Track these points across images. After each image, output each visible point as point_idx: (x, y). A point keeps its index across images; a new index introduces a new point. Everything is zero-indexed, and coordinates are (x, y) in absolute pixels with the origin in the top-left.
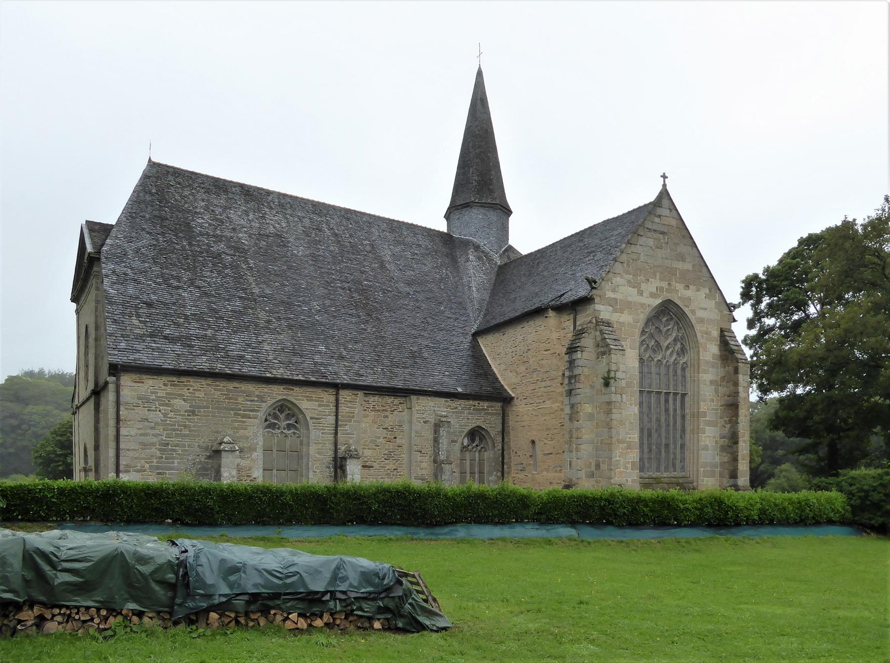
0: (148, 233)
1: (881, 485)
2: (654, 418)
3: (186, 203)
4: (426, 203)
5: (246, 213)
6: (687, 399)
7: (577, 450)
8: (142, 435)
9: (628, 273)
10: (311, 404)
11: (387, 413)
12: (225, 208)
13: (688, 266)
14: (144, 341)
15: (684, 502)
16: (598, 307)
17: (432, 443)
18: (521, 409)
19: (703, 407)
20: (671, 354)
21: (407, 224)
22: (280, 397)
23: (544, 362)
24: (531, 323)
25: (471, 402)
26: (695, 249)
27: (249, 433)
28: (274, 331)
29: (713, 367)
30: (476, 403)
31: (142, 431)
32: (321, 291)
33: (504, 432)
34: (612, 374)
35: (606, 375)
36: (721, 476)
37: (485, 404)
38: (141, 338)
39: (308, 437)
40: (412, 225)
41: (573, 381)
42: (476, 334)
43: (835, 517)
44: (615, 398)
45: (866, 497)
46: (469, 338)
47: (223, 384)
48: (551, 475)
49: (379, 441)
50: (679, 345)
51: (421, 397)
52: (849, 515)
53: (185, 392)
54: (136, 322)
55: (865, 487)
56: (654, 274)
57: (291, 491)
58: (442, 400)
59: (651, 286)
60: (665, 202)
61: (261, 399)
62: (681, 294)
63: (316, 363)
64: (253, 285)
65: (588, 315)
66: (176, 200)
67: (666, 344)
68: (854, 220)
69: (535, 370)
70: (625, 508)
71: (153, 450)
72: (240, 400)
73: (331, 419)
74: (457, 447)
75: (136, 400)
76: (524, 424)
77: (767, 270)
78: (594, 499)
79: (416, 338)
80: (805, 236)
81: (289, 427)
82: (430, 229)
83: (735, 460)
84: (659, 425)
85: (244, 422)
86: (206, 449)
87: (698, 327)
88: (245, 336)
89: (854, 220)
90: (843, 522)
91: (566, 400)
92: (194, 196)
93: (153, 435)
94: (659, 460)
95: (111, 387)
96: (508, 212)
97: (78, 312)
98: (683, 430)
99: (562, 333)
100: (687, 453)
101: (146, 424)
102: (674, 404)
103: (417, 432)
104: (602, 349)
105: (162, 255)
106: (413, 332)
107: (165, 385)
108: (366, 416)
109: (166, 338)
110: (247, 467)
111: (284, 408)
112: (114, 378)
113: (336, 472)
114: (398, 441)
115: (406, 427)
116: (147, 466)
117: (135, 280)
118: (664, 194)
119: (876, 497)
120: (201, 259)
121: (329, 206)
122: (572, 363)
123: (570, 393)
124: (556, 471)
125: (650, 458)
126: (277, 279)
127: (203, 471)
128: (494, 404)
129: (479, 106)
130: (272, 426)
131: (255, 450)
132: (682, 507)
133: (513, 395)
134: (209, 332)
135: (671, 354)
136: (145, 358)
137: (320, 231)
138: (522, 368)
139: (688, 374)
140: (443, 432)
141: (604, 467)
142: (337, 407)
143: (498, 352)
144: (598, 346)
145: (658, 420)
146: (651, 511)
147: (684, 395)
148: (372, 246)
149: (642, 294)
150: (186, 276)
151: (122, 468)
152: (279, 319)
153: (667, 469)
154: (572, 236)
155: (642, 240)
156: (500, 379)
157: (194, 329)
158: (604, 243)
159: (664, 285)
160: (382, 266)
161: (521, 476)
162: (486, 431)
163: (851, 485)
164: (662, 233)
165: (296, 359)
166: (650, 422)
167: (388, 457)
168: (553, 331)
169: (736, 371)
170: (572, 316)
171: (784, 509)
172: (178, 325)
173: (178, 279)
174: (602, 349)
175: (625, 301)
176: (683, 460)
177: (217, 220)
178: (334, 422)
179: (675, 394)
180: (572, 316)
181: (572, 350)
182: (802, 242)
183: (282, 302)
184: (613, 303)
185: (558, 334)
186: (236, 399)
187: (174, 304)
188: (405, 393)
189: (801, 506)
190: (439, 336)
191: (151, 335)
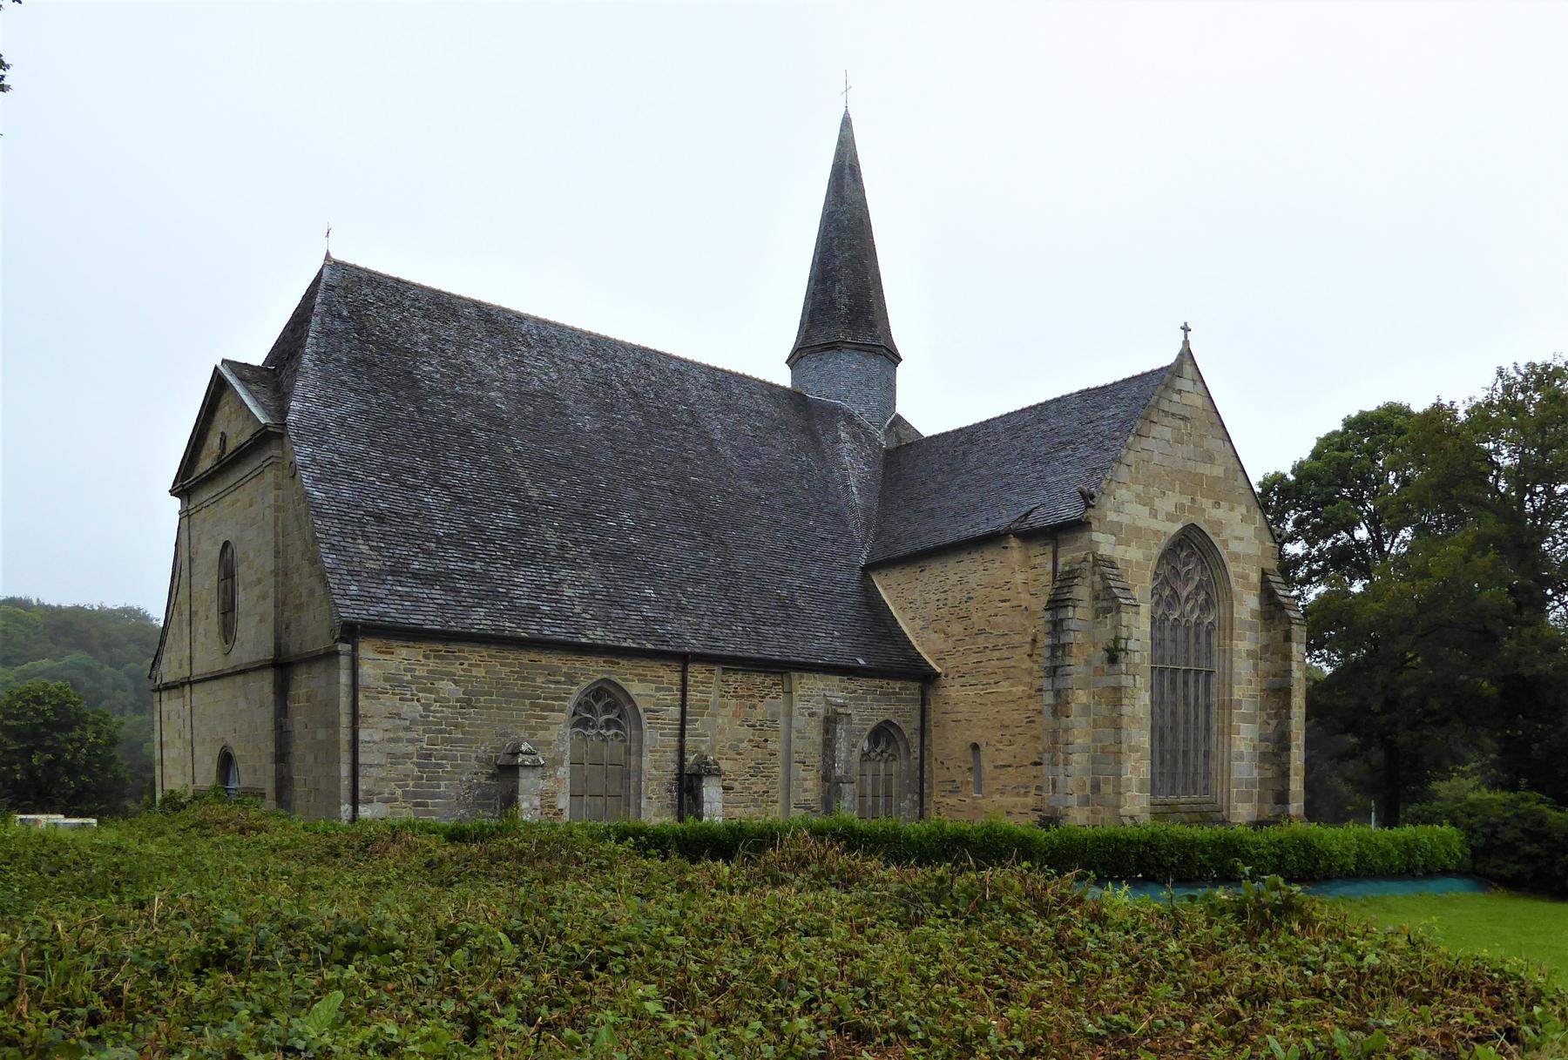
0: (352, 390)
1: (1517, 816)
2: (1168, 710)
3: (398, 335)
4: (751, 331)
5: (493, 355)
6: (1214, 680)
7: (1067, 763)
8: (391, 740)
9: (1136, 482)
10: (647, 688)
11: (755, 701)
12: (461, 346)
13: (1218, 471)
14: (384, 582)
15: (1257, 845)
16: (1097, 536)
17: (820, 749)
18: (954, 693)
19: (1238, 693)
20: (1192, 611)
21: (737, 374)
22: (599, 676)
23: (999, 619)
24: (977, 555)
25: (877, 682)
27: (552, 735)
28: (572, 564)
29: (1251, 629)
30: (884, 682)
31: (391, 735)
32: (631, 494)
33: (923, 731)
34: (1122, 644)
35: (1111, 645)
36: (1261, 800)
37: (897, 685)
38: (377, 576)
39: (640, 741)
40: (743, 376)
41: (1059, 653)
42: (869, 568)
43: (1452, 864)
44: (1126, 681)
45: (1494, 834)
46: (858, 573)
47: (511, 656)
48: (1008, 800)
50: (1202, 597)
52: (1468, 862)
53: (456, 668)
54: (365, 549)
55: (1493, 820)
56: (1172, 482)
57: (676, 837)
58: (835, 680)
59: (1167, 505)
60: (1188, 369)
61: (571, 680)
63: (646, 619)
64: (527, 484)
65: (1078, 549)
66: (382, 331)
67: (1185, 594)
68: (1452, 403)
69: (982, 632)
70: (1173, 855)
71: (409, 765)
72: (539, 680)
73: (675, 711)
74: (857, 753)
75: (382, 683)
76: (959, 717)
77: (1298, 469)
78: (1130, 842)
79: (782, 573)
80: (1354, 414)
81: (609, 724)
82: (771, 385)
83: (1285, 775)
84: (1175, 721)
85: (544, 718)
86: (488, 762)
87: (1232, 568)
88: (531, 571)
89: (1452, 403)
90: (1460, 873)
91: (1046, 683)
92: (409, 323)
93: (409, 741)
94: (1173, 776)
95: (344, 661)
96: (895, 359)
97: (185, 514)
98: (1208, 729)
99: (1031, 574)
100: (1212, 765)
101: (398, 722)
102: (1196, 688)
103: (799, 731)
104: (1105, 604)
105: (381, 429)
106: (776, 563)
107: (426, 657)
108: (724, 706)
109: (415, 575)
112: (349, 647)
113: (680, 798)
114: (770, 746)
115: (782, 723)
116: (399, 792)
117: (350, 474)
118: (1186, 356)
119: (1509, 834)
120: (441, 437)
121: (615, 342)
122: (1057, 626)
123: (1053, 672)
124: (1018, 794)
125: (1162, 774)
126: (563, 473)
127: (483, 800)
128: (909, 684)
129: (848, 178)
130: (584, 723)
131: (561, 763)
132: (1254, 852)
133: (939, 670)
134: (477, 565)
135: (1192, 611)
136: (393, 612)
137: (610, 386)
138: (957, 628)
139: (1214, 641)
140: (840, 731)
141: (1107, 789)
142: (684, 691)
143: (910, 601)
144: (1096, 598)
145: (1174, 713)
146: (1210, 859)
147: (1209, 674)
148: (691, 413)
149: (1155, 516)
150: (424, 466)
151: (361, 795)
152: (576, 543)
153: (1185, 792)
154: (1023, 410)
155: (1156, 430)
156: (914, 643)
157: (454, 561)
158: (1088, 429)
159: (1186, 500)
160: (712, 450)
161: (952, 800)
162: (899, 729)
163: (1470, 816)
164: (1184, 418)
165: (617, 612)
166: (1162, 716)
167: (756, 771)
168: (1018, 574)
169: (1288, 638)
170: (1050, 549)
171: (1388, 853)
172: (429, 554)
173: (414, 472)
174: (1105, 604)
175: (1132, 526)
176: (1207, 775)
177: (452, 366)
178: (678, 716)
179: (1198, 672)
180: (1050, 549)
181: (1057, 603)
182: (1349, 423)
183: (576, 512)
184: (1115, 529)
185: (1023, 576)
186: (534, 680)
187: (415, 516)
188: (781, 668)
189: (1409, 848)
190: (815, 570)
191: (392, 573)
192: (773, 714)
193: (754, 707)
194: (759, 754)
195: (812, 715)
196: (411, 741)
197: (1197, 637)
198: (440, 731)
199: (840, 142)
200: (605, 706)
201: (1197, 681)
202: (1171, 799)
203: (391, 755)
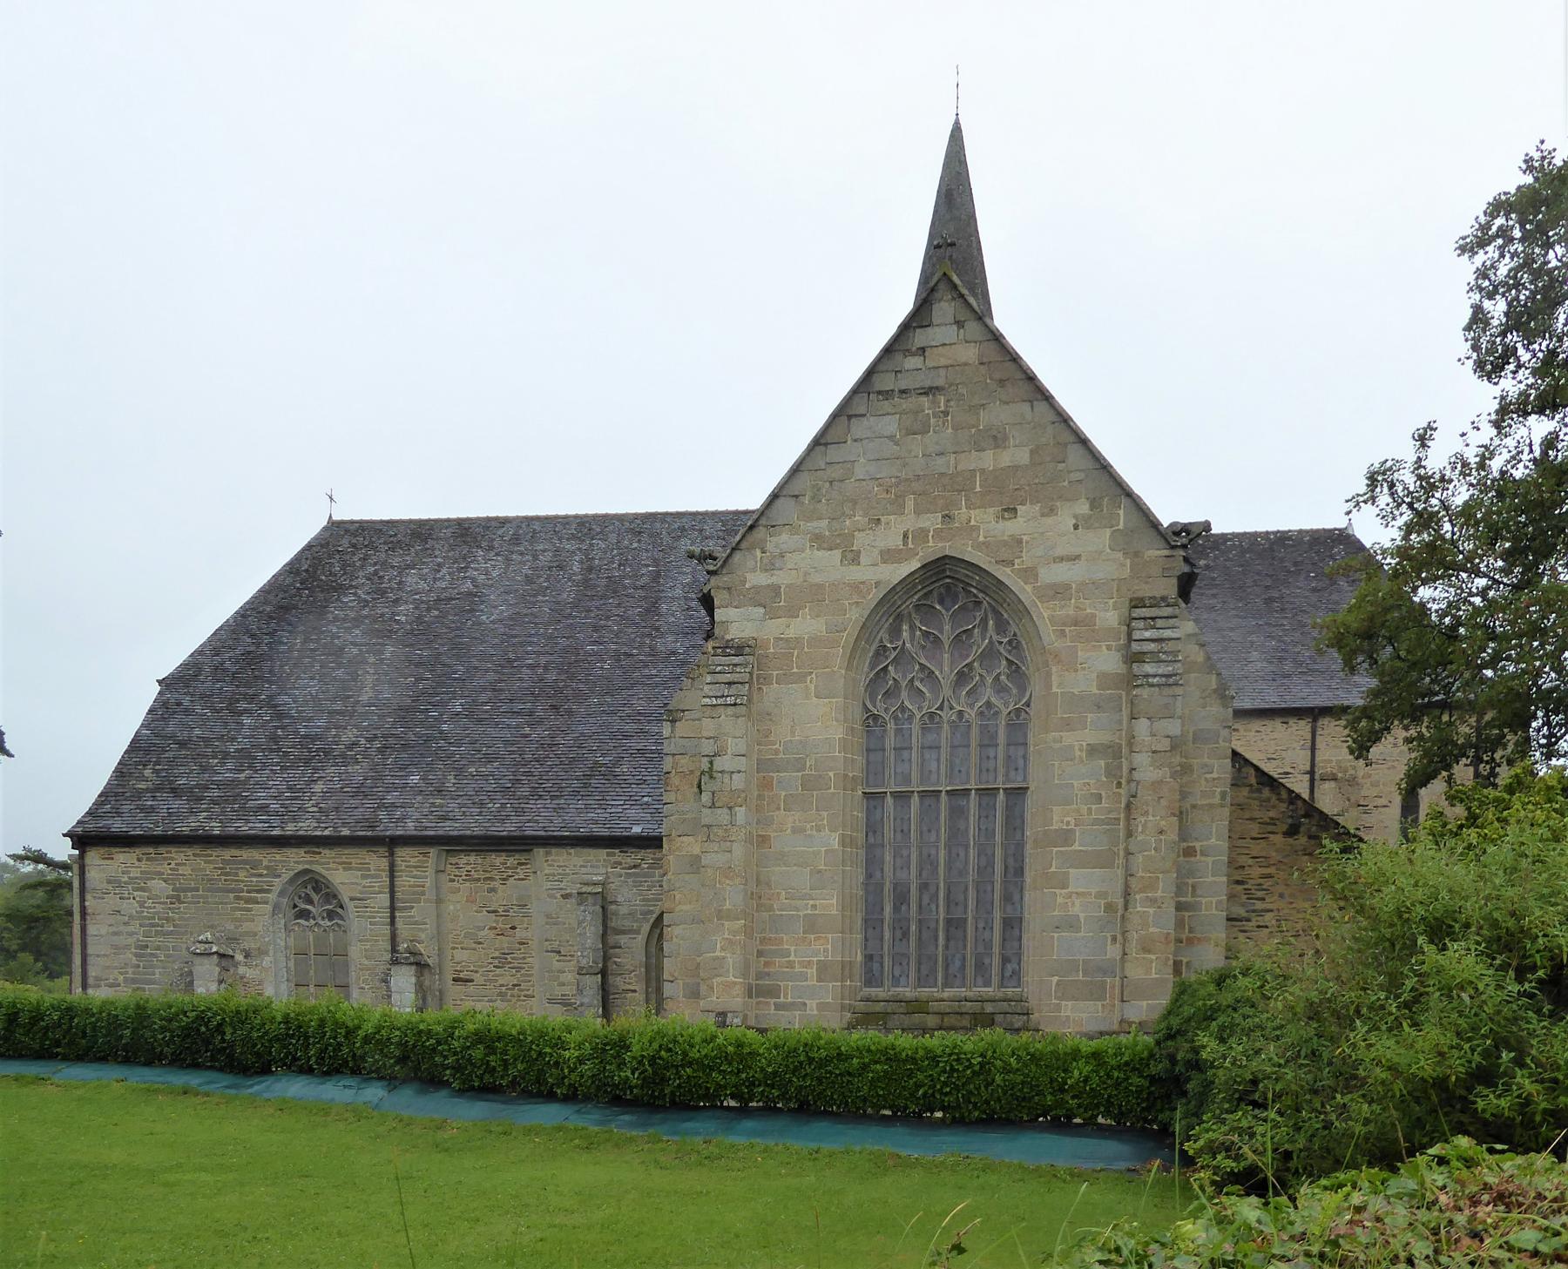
8: (115, 934)
10: (349, 875)
11: (496, 884)
13: (1016, 455)
22: (301, 867)
26: (1041, 407)
49: (482, 933)
51: (554, 850)
53: (165, 868)
58: (602, 853)
62: (980, 534)
72: (242, 875)
73: (385, 899)
85: (249, 910)
110: (272, 984)
111: (313, 885)
114: (520, 934)
131: (266, 953)
142: (392, 877)
147: (1018, 793)
149: (855, 560)
151: (91, 981)
184: (768, 599)
196: (131, 934)
198: (152, 925)
199: (952, 136)
200: (313, 896)
202: (924, 992)
203: (116, 947)
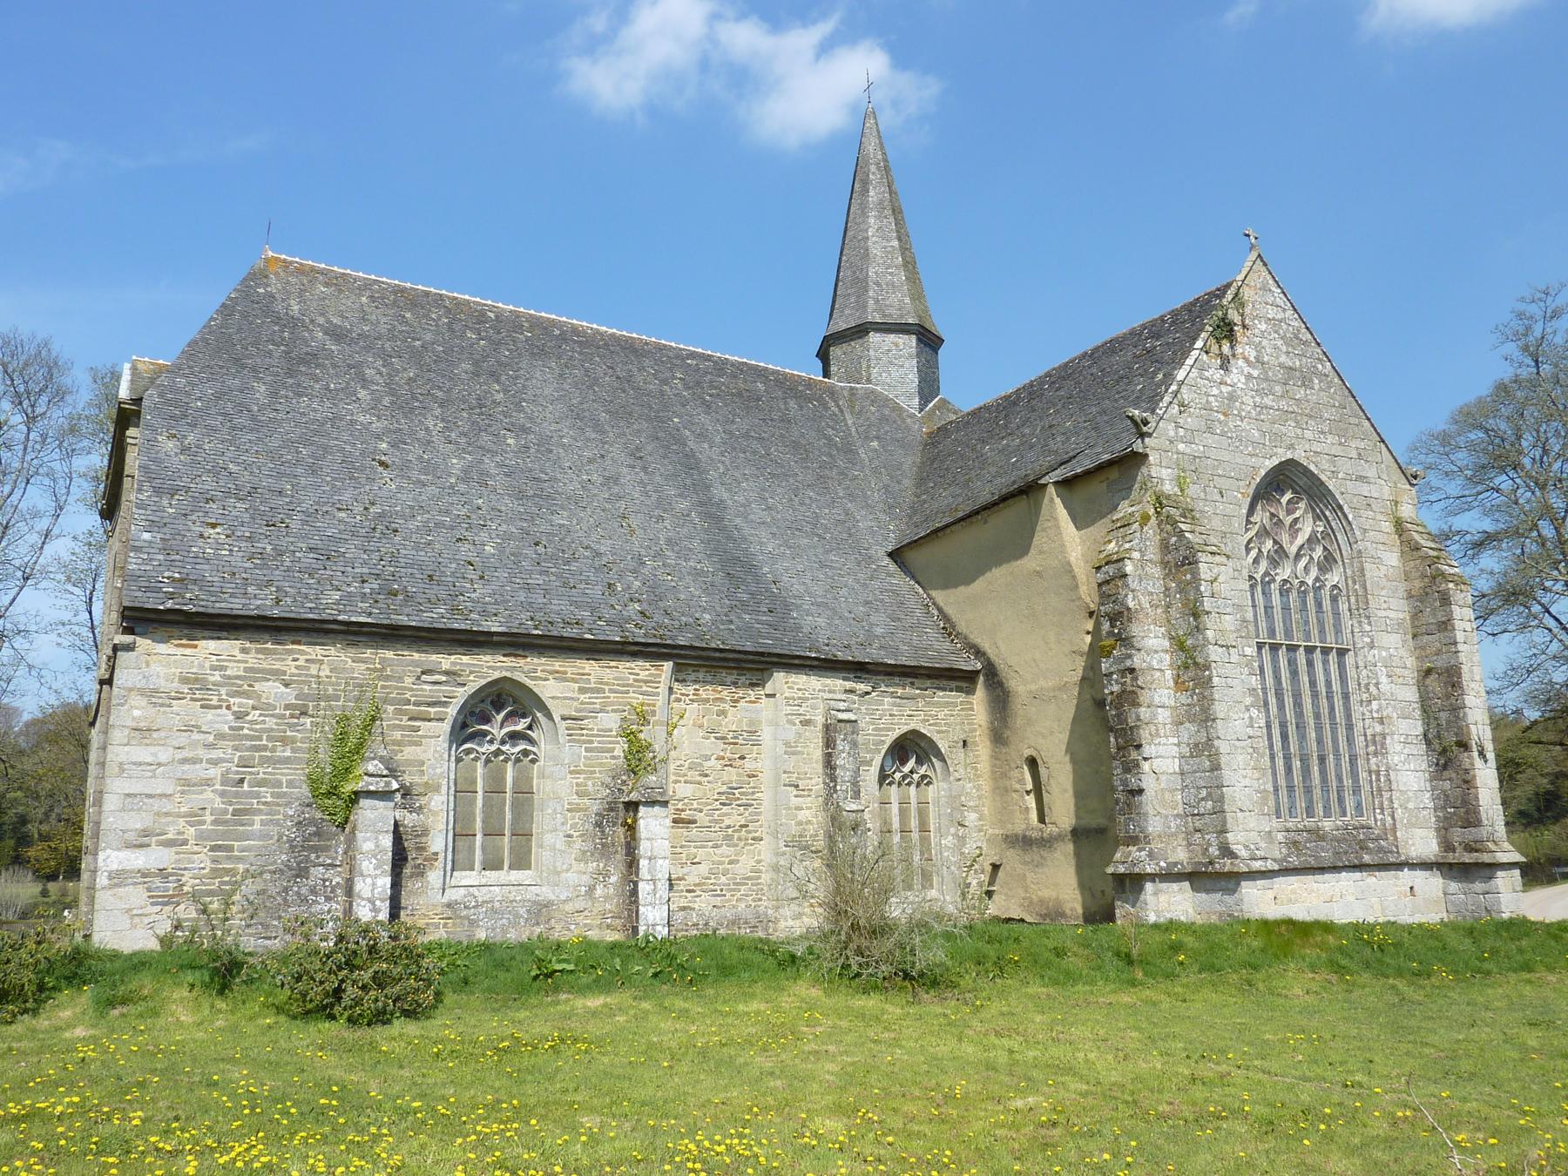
8: (185, 761)
50: (1318, 553)
67: (1293, 550)
71: (209, 794)
72: (408, 681)
101: (196, 736)
102: (1327, 672)
162: (930, 741)
186: (401, 679)
192: (751, 723)
193: (723, 713)
194: (731, 775)
195: (806, 723)
196: (214, 762)
197: (1319, 605)
201: (1325, 662)
203: (187, 783)
